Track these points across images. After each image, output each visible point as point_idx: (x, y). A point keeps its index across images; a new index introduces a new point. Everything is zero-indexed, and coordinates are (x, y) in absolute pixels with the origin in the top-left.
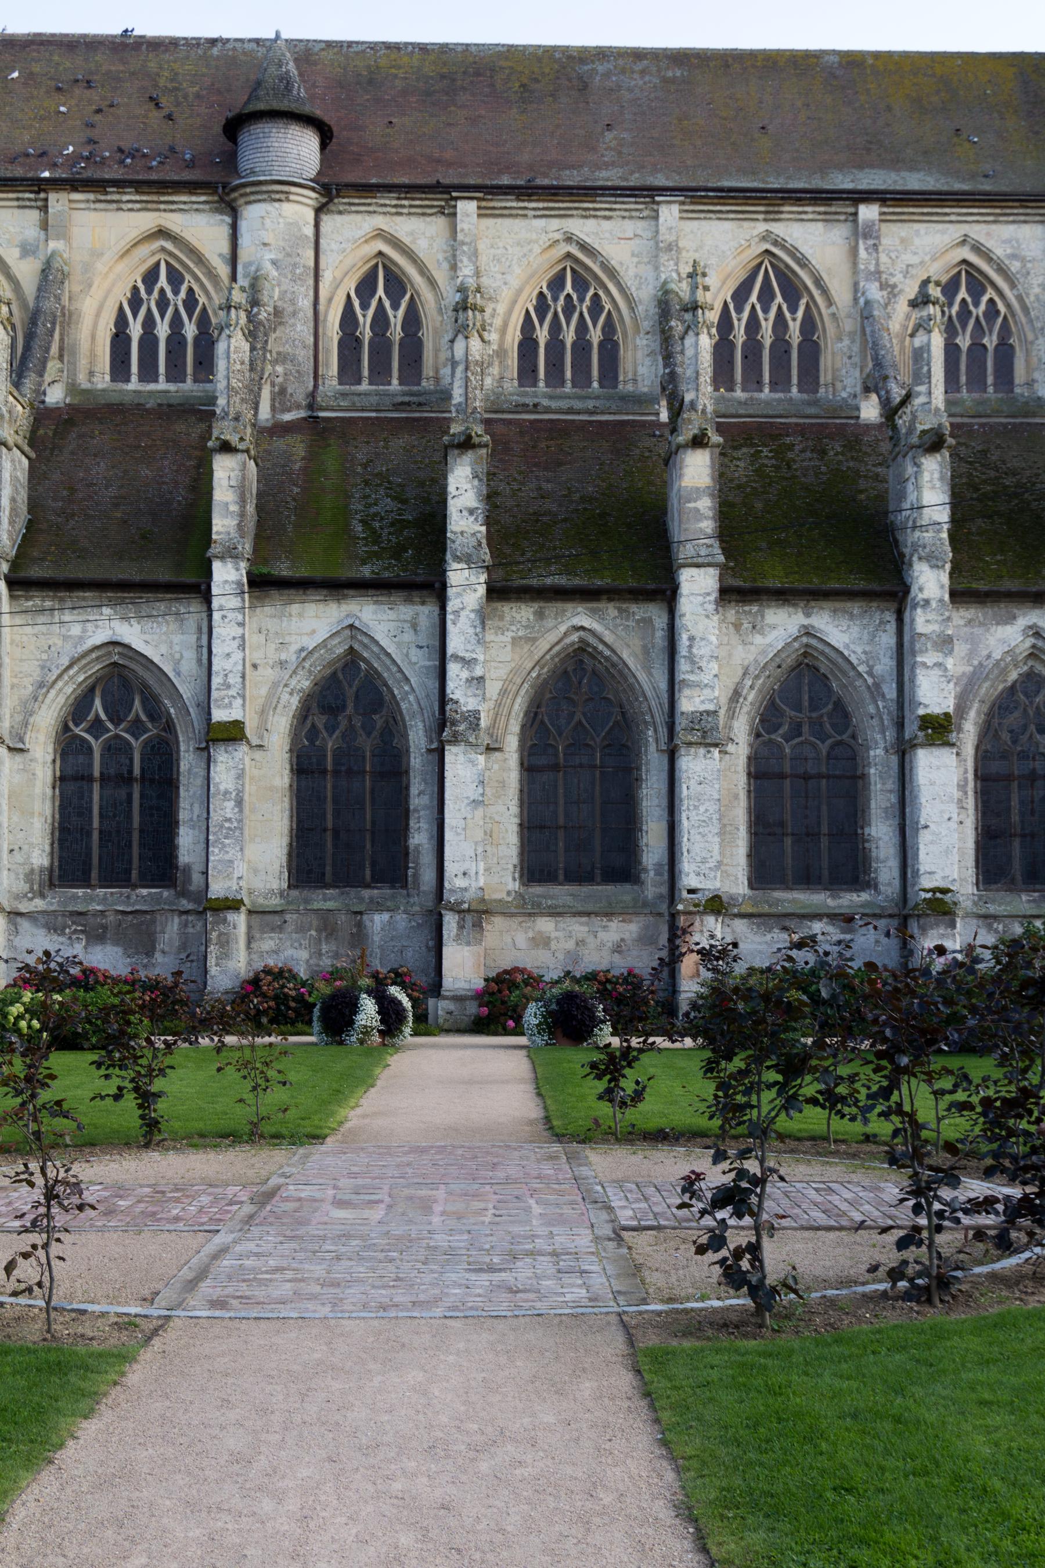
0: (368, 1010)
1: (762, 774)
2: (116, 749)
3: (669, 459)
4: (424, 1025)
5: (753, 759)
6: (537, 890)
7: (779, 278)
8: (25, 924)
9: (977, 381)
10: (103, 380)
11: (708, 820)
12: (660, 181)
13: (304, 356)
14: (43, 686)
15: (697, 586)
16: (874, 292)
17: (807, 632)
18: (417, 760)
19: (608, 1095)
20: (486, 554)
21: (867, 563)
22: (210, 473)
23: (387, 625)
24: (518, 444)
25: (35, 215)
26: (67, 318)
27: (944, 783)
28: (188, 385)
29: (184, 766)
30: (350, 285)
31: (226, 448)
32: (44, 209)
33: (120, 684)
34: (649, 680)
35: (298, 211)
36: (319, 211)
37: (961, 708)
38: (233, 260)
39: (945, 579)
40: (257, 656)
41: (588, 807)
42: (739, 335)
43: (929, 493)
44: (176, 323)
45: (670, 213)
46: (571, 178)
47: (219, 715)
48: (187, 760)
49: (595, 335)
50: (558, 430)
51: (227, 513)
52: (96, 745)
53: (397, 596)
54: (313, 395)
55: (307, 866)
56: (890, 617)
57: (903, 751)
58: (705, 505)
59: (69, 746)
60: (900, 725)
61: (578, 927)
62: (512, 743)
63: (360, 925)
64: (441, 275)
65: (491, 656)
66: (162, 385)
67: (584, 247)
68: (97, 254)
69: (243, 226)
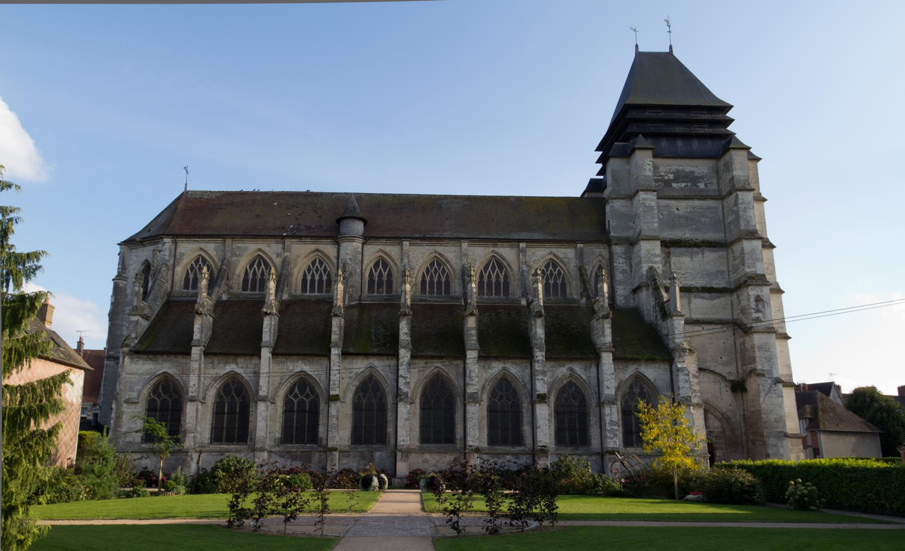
0: (376, 481)
1: (491, 411)
2: (302, 403)
3: (463, 319)
4: (391, 486)
5: (489, 406)
6: (425, 445)
7: (497, 263)
8: (273, 455)
9: (555, 293)
10: (299, 292)
11: (475, 426)
12: (462, 236)
13: (358, 285)
14: (281, 384)
15: (472, 355)
16: (525, 268)
17: (504, 369)
18: (390, 406)
19: (438, 500)
20: (410, 346)
21: (522, 349)
22: (331, 323)
23: (380, 365)
24: (420, 310)
25: (281, 245)
26: (290, 274)
27: (544, 413)
28: (324, 294)
29: (321, 408)
30: (372, 265)
31: (336, 315)
32: (284, 244)
33: (303, 383)
34: (458, 383)
35: (357, 244)
36: (363, 244)
37: (549, 392)
38: (338, 258)
39: (544, 354)
40: (344, 375)
41: (439, 424)
42: (486, 279)
43: (539, 331)
44: (321, 276)
45: (465, 245)
46: (436, 235)
47: (332, 393)
48: (322, 406)
49: (443, 279)
50: (432, 307)
51: (336, 334)
52: (296, 401)
53: (385, 358)
54: (360, 297)
55: (357, 438)
56: (528, 365)
57: (533, 404)
58: (474, 332)
59: (288, 402)
60: (532, 397)
61: (437, 457)
62: (418, 401)
63: (372, 456)
64: (398, 262)
65: (410, 375)
66: (316, 294)
67: (440, 254)
68: (298, 256)
69: (341, 248)
